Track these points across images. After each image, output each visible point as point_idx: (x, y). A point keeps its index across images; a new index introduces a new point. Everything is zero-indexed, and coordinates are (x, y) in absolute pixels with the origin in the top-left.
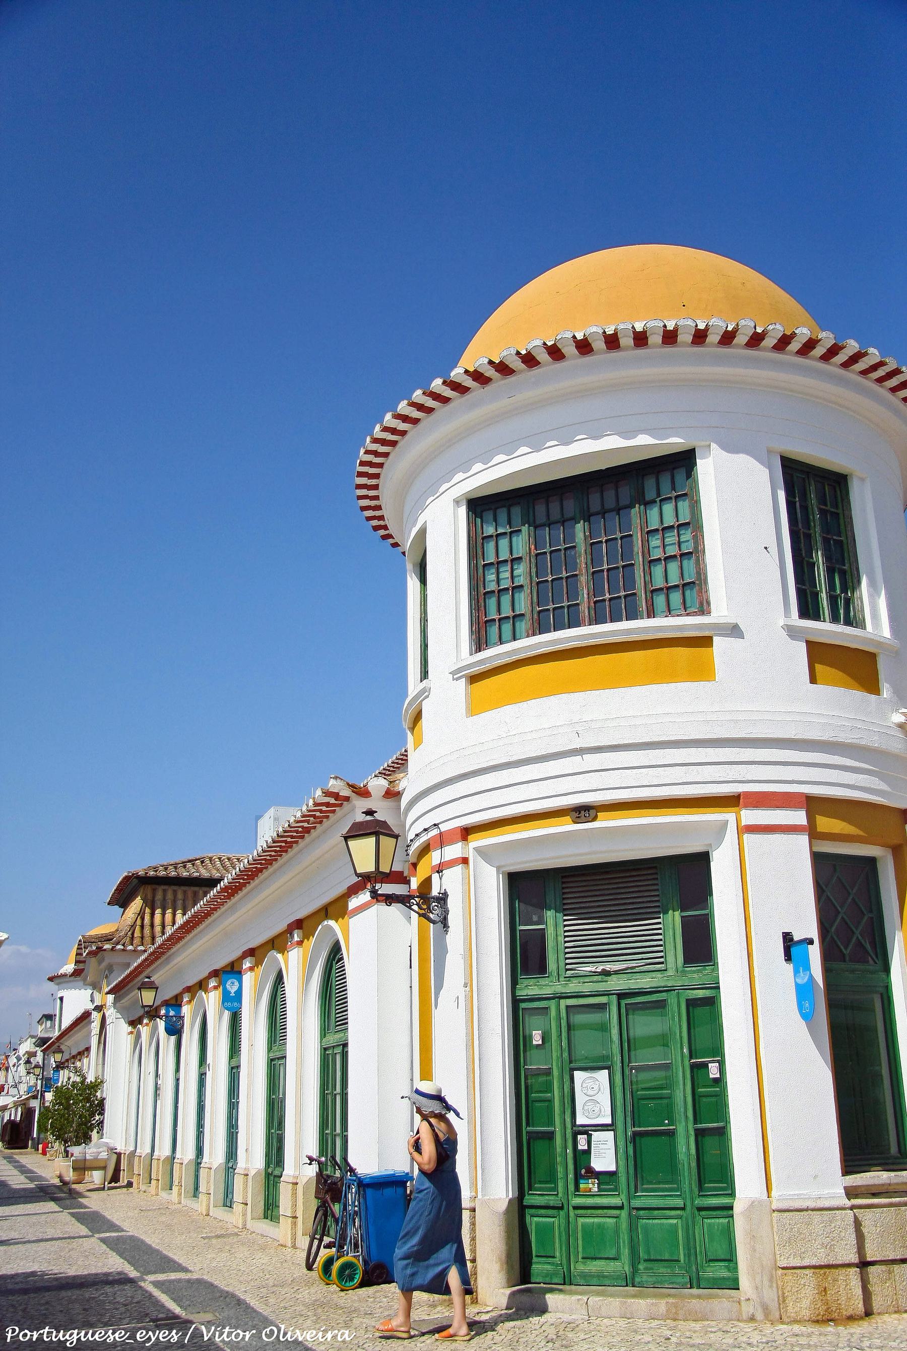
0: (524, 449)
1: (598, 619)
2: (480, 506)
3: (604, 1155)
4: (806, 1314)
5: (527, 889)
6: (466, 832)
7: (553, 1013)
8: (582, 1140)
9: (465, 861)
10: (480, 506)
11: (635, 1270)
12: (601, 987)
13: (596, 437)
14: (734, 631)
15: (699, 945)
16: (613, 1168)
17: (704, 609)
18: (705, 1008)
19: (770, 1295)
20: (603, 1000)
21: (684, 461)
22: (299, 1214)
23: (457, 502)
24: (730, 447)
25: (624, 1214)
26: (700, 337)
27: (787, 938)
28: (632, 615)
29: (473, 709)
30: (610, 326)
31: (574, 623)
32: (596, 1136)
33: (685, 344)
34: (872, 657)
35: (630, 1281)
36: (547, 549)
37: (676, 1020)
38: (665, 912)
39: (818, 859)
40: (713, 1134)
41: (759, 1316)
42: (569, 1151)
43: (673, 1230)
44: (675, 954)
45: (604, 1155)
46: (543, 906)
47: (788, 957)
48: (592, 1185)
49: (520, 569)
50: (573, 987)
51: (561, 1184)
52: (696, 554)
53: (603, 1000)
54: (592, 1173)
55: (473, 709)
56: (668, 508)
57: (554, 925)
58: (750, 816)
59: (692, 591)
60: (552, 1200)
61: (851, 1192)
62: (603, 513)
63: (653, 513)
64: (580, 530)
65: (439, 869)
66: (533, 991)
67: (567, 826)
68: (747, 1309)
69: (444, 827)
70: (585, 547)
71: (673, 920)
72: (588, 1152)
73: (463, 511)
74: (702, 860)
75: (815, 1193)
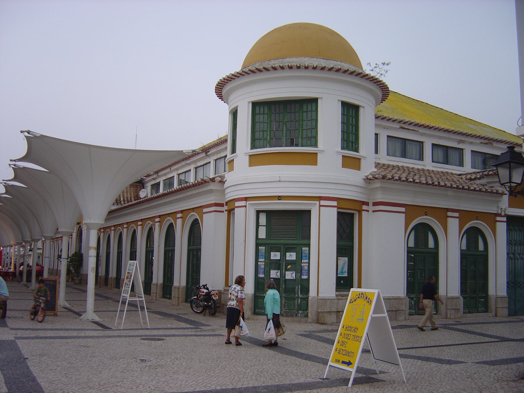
2: (255, 105)
9: (246, 206)
10: (255, 105)
17: (316, 145)
22: (180, 296)
34: (360, 159)
39: (339, 213)
55: (251, 165)
59: (313, 141)
61: (337, 295)
74: (309, 212)
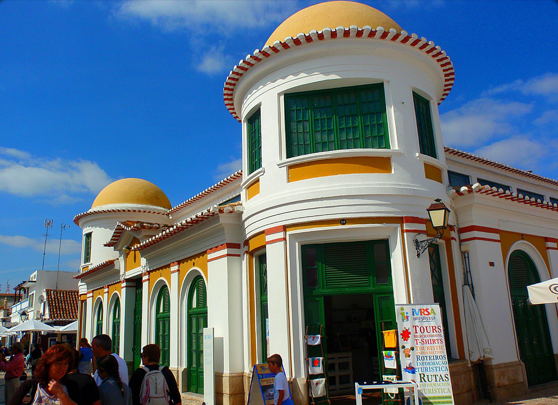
6: (285, 228)
9: (285, 239)
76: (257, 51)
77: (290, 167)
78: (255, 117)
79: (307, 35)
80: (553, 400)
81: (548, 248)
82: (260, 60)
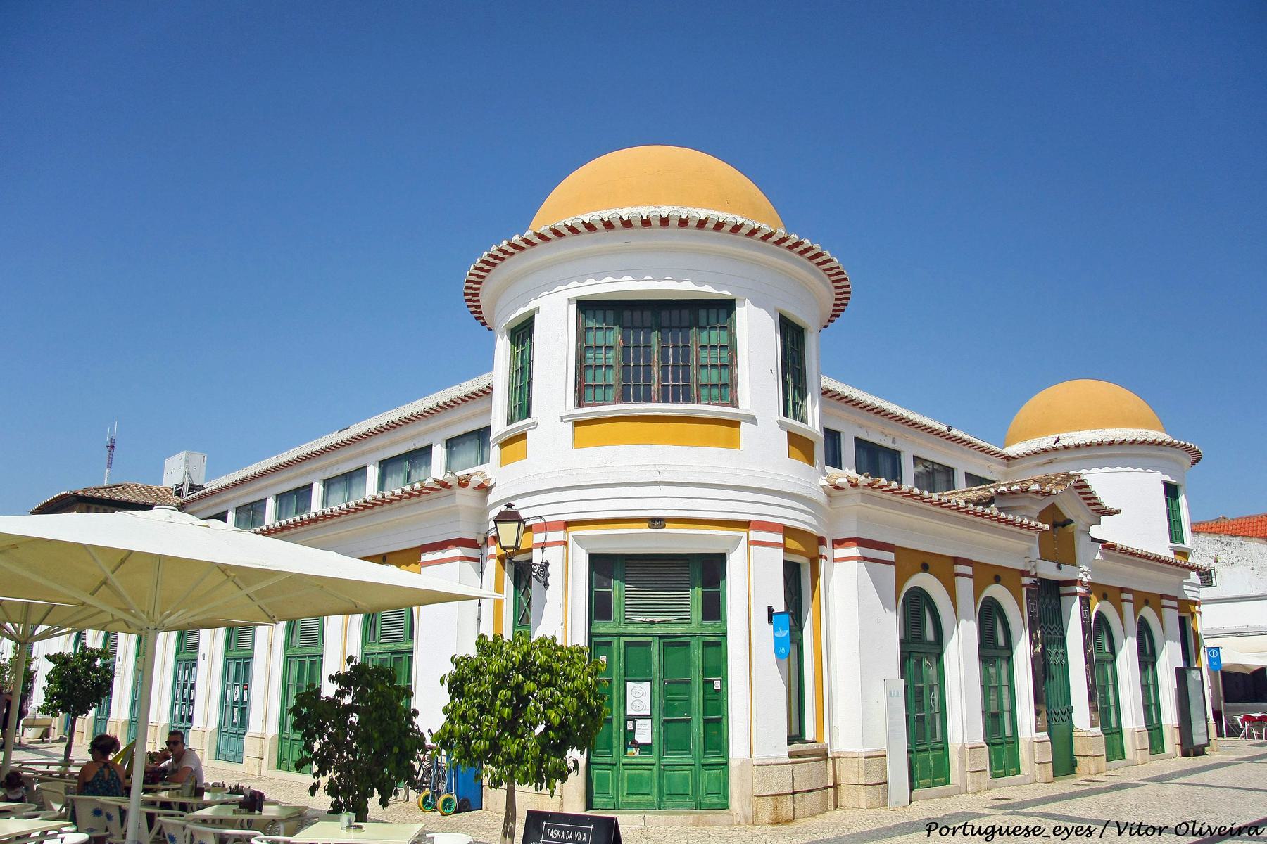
0: (629, 278)
1: (665, 400)
2: (586, 306)
3: (644, 733)
4: (767, 820)
5: (604, 566)
6: (568, 524)
7: (615, 645)
8: (630, 724)
9: (565, 543)
10: (586, 306)
11: (661, 800)
12: (649, 631)
13: (679, 281)
14: (753, 420)
15: (714, 609)
16: (649, 741)
17: (734, 403)
18: (717, 646)
19: (749, 811)
20: (650, 639)
21: (727, 307)
23: (569, 300)
24: (756, 304)
25: (655, 768)
26: (736, 229)
27: (770, 610)
28: (687, 400)
29: (577, 443)
30: (649, 199)
31: (648, 399)
32: (639, 722)
33: (692, 227)
35: (659, 807)
36: (680, 344)
37: (696, 652)
38: (693, 588)
39: (786, 562)
40: (716, 724)
41: (743, 822)
42: (622, 730)
43: (686, 777)
44: (697, 613)
45: (644, 733)
46: (611, 577)
47: (770, 620)
48: (636, 751)
49: (611, 354)
50: (631, 629)
51: (615, 750)
52: (731, 366)
53: (650, 639)
54: (635, 744)
55: (577, 443)
56: (713, 334)
57: (619, 590)
58: (755, 535)
59: (727, 391)
60: (608, 760)
61: (791, 755)
62: (670, 328)
63: (704, 335)
64: (655, 337)
65: (543, 546)
66: (603, 631)
67: (645, 529)
68: (736, 819)
69: (548, 519)
70: (654, 349)
71: (698, 592)
72: (634, 731)
73: (574, 307)
75: (774, 755)
76: (505, 242)
77: (577, 424)
78: (523, 333)
79: (625, 218)
80: (843, 768)
81: (958, 574)
82: (534, 244)
